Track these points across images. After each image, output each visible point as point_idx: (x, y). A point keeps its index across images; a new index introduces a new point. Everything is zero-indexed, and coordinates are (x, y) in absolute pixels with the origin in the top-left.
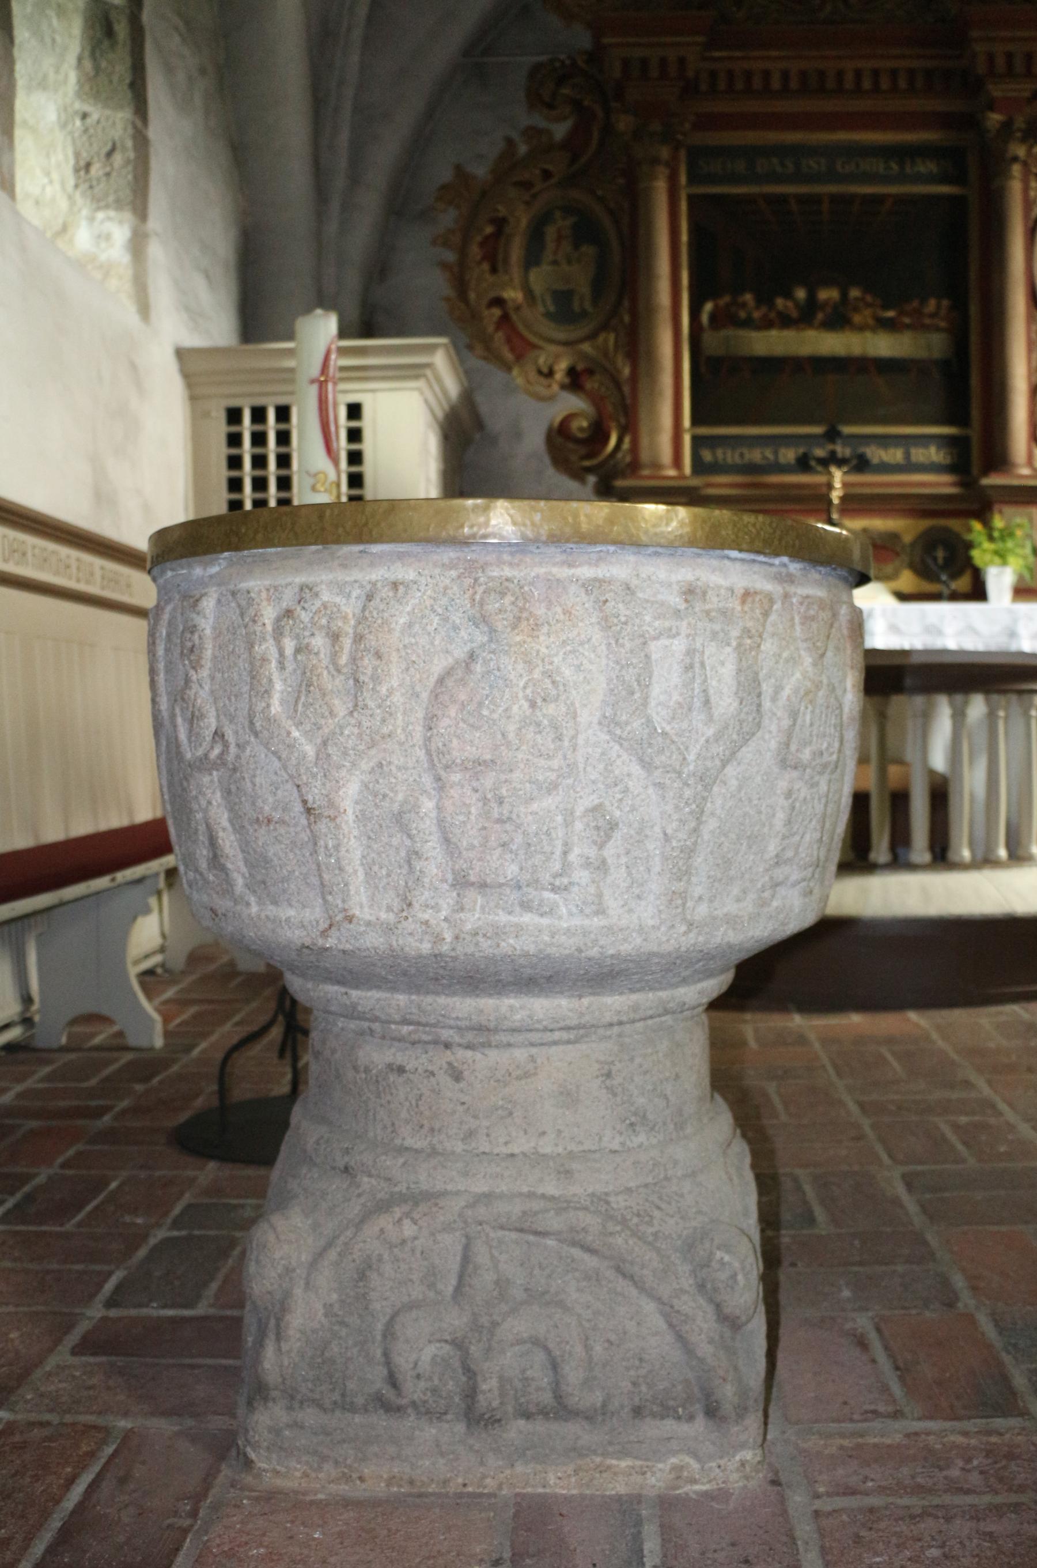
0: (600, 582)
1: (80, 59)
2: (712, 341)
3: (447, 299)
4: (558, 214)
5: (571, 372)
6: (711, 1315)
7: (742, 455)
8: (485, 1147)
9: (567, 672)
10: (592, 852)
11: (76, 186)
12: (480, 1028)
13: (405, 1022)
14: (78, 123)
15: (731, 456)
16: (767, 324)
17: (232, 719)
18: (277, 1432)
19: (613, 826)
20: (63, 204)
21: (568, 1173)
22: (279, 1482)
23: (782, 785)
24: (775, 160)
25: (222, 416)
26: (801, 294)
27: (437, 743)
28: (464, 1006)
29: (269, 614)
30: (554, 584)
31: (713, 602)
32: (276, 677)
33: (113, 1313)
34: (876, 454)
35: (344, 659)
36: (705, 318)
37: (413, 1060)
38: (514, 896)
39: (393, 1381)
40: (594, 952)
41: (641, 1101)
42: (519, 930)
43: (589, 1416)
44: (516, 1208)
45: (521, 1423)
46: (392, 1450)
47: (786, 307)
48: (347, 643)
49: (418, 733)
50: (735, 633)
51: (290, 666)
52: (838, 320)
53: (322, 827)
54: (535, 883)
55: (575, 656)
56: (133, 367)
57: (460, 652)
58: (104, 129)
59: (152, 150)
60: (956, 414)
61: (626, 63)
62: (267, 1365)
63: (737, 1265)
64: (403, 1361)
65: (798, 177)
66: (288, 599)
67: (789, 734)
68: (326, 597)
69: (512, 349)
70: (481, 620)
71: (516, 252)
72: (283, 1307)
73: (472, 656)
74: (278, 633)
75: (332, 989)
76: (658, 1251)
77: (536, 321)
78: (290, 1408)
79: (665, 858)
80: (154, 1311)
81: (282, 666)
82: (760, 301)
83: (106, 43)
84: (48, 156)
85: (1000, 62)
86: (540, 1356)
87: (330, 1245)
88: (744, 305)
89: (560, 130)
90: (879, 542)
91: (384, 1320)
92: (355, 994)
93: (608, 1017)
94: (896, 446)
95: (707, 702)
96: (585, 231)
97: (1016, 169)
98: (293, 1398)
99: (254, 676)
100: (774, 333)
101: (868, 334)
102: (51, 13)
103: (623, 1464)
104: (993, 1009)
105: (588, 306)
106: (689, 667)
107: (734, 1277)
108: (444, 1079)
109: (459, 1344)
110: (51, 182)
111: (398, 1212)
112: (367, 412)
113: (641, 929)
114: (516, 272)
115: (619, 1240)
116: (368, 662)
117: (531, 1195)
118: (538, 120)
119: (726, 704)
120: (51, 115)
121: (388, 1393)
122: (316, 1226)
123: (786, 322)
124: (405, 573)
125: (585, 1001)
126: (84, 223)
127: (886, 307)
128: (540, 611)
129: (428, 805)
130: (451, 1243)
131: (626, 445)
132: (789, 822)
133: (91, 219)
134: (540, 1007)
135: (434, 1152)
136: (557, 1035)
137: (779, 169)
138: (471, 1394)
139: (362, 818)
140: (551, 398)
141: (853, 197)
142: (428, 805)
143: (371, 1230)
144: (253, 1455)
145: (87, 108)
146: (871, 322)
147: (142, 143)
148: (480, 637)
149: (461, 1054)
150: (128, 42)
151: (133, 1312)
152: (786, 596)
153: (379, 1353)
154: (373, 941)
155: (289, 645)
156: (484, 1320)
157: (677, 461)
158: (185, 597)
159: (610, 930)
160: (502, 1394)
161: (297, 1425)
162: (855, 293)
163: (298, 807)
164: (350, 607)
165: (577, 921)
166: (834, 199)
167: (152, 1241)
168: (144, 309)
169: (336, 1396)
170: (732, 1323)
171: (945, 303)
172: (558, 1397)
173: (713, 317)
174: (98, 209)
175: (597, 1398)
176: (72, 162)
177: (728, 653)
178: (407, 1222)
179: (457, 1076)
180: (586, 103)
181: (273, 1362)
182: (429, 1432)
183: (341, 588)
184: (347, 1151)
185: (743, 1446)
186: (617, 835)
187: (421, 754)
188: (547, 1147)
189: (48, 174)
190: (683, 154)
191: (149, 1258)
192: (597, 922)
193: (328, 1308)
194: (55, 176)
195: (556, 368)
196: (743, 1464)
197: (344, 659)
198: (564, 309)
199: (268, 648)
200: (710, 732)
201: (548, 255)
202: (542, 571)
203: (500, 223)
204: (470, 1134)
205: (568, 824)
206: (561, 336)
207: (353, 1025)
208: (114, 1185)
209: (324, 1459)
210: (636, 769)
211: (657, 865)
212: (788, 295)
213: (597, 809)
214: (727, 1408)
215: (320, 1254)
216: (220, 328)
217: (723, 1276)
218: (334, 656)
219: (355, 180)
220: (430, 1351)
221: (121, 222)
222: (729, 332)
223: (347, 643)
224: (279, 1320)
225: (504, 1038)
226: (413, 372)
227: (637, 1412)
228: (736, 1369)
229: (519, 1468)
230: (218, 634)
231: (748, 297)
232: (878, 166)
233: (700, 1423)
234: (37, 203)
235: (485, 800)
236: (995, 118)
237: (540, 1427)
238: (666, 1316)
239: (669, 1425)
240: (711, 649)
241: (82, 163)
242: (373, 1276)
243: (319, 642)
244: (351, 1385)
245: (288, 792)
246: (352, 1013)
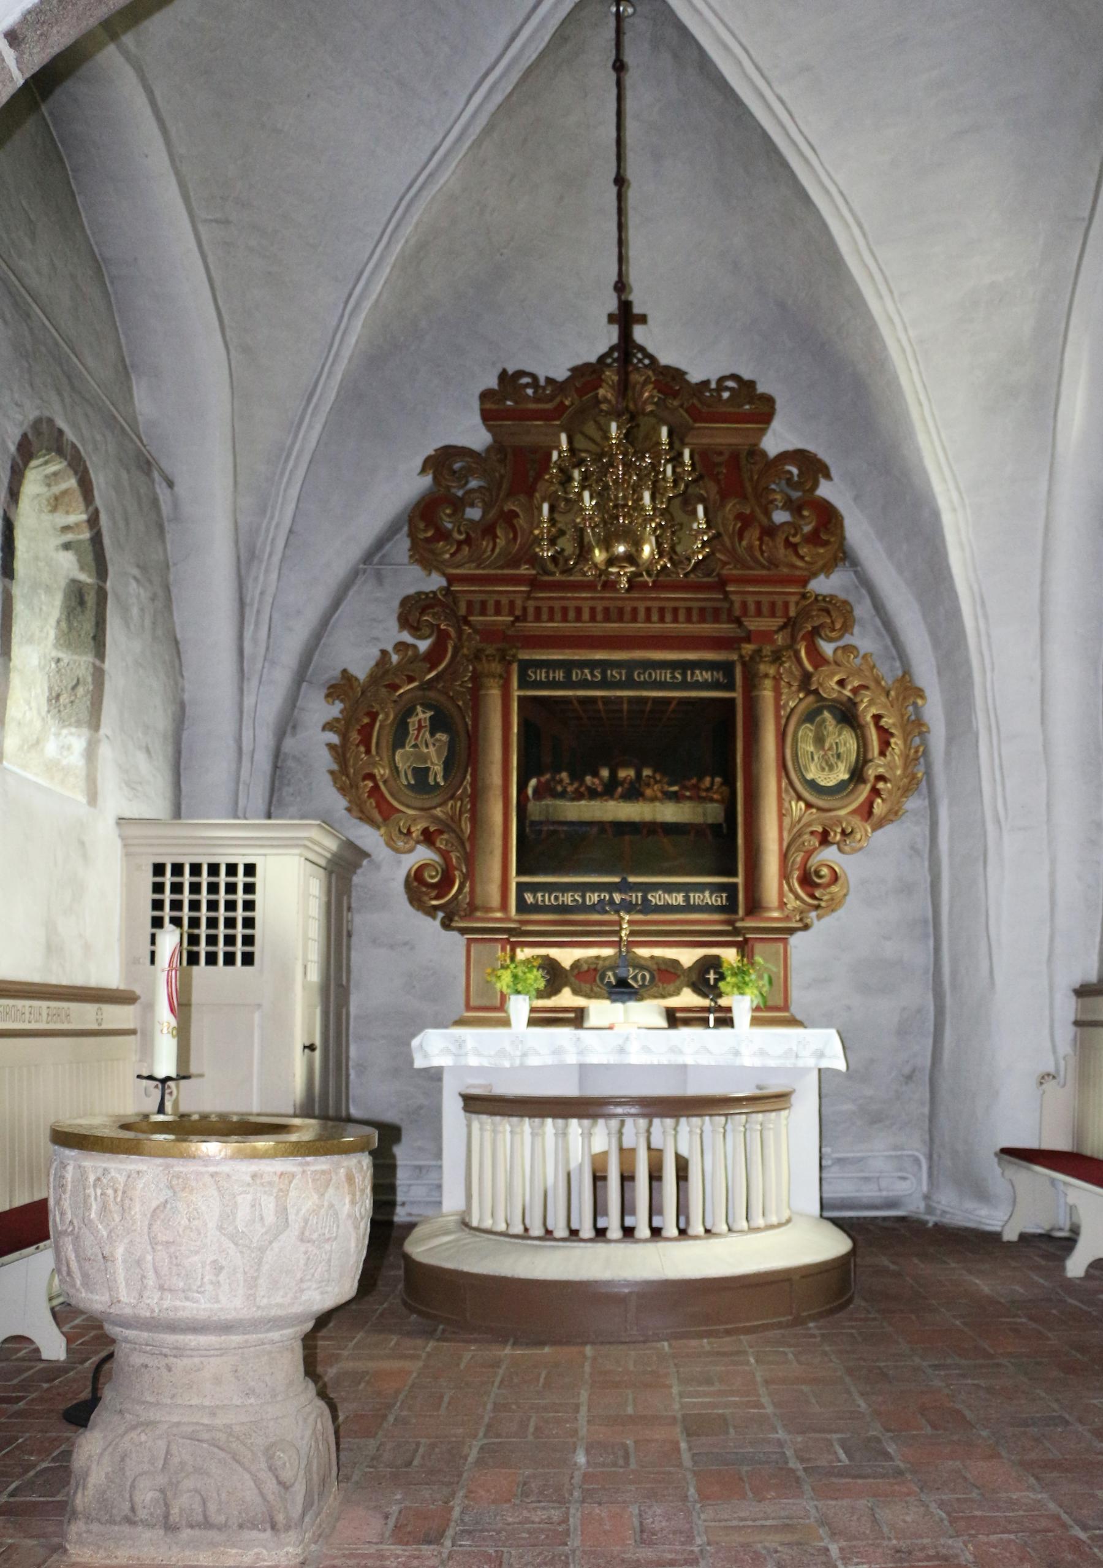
0: (216, 1173)
1: (58, 622)
2: (535, 809)
3: (332, 773)
4: (419, 709)
5: (425, 832)
6: (274, 1481)
7: (556, 898)
8: (179, 1402)
9: (203, 1208)
10: (214, 1279)
11: (49, 711)
12: (176, 1348)
13: (147, 1345)
14: (53, 665)
15: (548, 899)
16: (578, 796)
17: (77, 1216)
18: (79, 1534)
19: (222, 1268)
20: (38, 724)
21: (214, 1414)
22: (79, 1560)
23: (303, 1249)
24: (587, 671)
25: (150, 870)
26: (605, 773)
27: (152, 1235)
28: (170, 1338)
29: (92, 1178)
30: (199, 1174)
31: (266, 1179)
32: (94, 1204)
33: (12, 1499)
35: (119, 1199)
36: (530, 791)
37: (151, 1362)
38: (182, 1295)
39: (133, 1509)
40: (215, 1318)
41: (252, 1384)
42: (184, 1308)
43: (220, 1528)
44: (190, 1429)
45: (189, 1530)
46: (130, 1542)
47: (594, 784)
48: (120, 1193)
49: (146, 1230)
50: (275, 1190)
51: (99, 1199)
52: (633, 793)
53: (109, 1264)
54: (190, 1289)
55: (206, 1204)
56: (82, 843)
57: (162, 1200)
58: (71, 670)
59: (106, 677)
61: (470, 604)
62: (77, 1502)
63: (286, 1459)
64: (138, 1499)
65: (604, 684)
66: (100, 1172)
67: (304, 1228)
68: (113, 1174)
69: (380, 812)
70: (171, 1187)
72: (86, 1474)
73: (166, 1201)
74: (95, 1186)
75: (118, 1329)
76: (252, 1451)
78: (86, 1523)
79: (245, 1281)
80: (34, 1498)
81: (96, 1199)
82: (573, 777)
83: (79, 609)
84: (30, 690)
85: (752, 608)
86: (198, 1498)
87: (110, 1444)
88: (561, 781)
89: (423, 645)
90: (663, 967)
91: (131, 1480)
92: (127, 1332)
93: (233, 1345)
94: (678, 891)
95: (262, 1219)
97: (768, 683)
98: (89, 1519)
99: (85, 1202)
100: (583, 802)
101: (657, 804)
102: (41, 592)
103: (234, 1551)
105: (440, 780)
106: (253, 1206)
107: (285, 1464)
108: (164, 1371)
109: (162, 1491)
110: (31, 709)
111: (139, 1430)
112: (259, 870)
113: (235, 1309)
114: (385, 754)
115: (234, 1445)
116: (127, 1202)
117: (197, 1423)
118: (406, 637)
119: (270, 1218)
120: (34, 661)
121: (130, 1514)
122: (105, 1437)
123: (593, 794)
124: (142, 1167)
125: (223, 1338)
126: (52, 738)
127: (671, 784)
128: (194, 1184)
129: (149, 1258)
130: (162, 1444)
131: (467, 889)
132: (306, 1264)
133: (57, 735)
134: (203, 1340)
135: (158, 1404)
136: (212, 1352)
137: (589, 677)
138: (167, 1516)
139: (124, 1261)
140: (411, 851)
141: (647, 698)
142: (149, 1258)
143: (127, 1438)
144: (68, 1547)
145: (61, 655)
146: (659, 795)
147: (99, 675)
148: (170, 1193)
149: (172, 1360)
150: (95, 606)
151: (22, 1499)
152: (304, 1172)
153: (128, 1496)
154: (128, 1311)
155: (99, 1192)
156: (174, 1480)
157: (504, 906)
158: (62, 1163)
159: (222, 1309)
160: (181, 1516)
161: (89, 1531)
162: (647, 772)
163: (100, 1256)
164: (121, 1179)
165: (208, 1305)
166: (631, 700)
167: (38, 1469)
168: (93, 797)
169: (107, 1517)
170: (284, 1486)
171: (718, 780)
172: (205, 1517)
173: (536, 791)
174: (64, 727)
175: (222, 1519)
176: (47, 694)
177: (272, 1199)
178: (143, 1435)
179: (169, 1369)
180: (442, 627)
181: (82, 1500)
182: (147, 1534)
183: (119, 1171)
184: (121, 1403)
185: (288, 1544)
186: (224, 1272)
187: (146, 1237)
188: (207, 1403)
189: (29, 703)
190: (515, 667)
191: (36, 1475)
192: (216, 1306)
193: (107, 1474)
194: (33, 704)
195: (413, 829)
196: (287, 1553)
197: (119, 1199)
199: (91, 1191)
200: (263, 1230)
201: (410, 741)
202: (195, 1168)
204: (173, 1396)
205: (203, 1267)
206: (418, 804)
207: (128, 1346)
208: (20, 1440)
209: (99, 1547)
210: (232, 1246)
211: (242, 1283)
212: (595, 774)
213: (215, 1261)
214: (280, 1526)
215: (105, 1450)
216: (153, 804)
217: (279, 1463)
218: (115, 1198)
220: (150, 1495)
221: (79, 736)
222: (548, 801)
223: (120, 1193)
224: (84, 1480)
225: (189, 1353)
227: (241, 1526)
228: (286, 1508)
229: (187, 1553)
230: (73, 1182)
231: (564, 775)
232: (667, 675)
233: (269, 1532)
234: (19, 724)
235: (171, 1257)
237: (197, 1532)
238: (255, 1482)
239: (254, 1534)
240: (264, 1197)
241: (54, 694)
242: (128, 1460)
243: (110, 1192)
244: (115, 1511)
245: (97, 1250)
246: (126, 1340)
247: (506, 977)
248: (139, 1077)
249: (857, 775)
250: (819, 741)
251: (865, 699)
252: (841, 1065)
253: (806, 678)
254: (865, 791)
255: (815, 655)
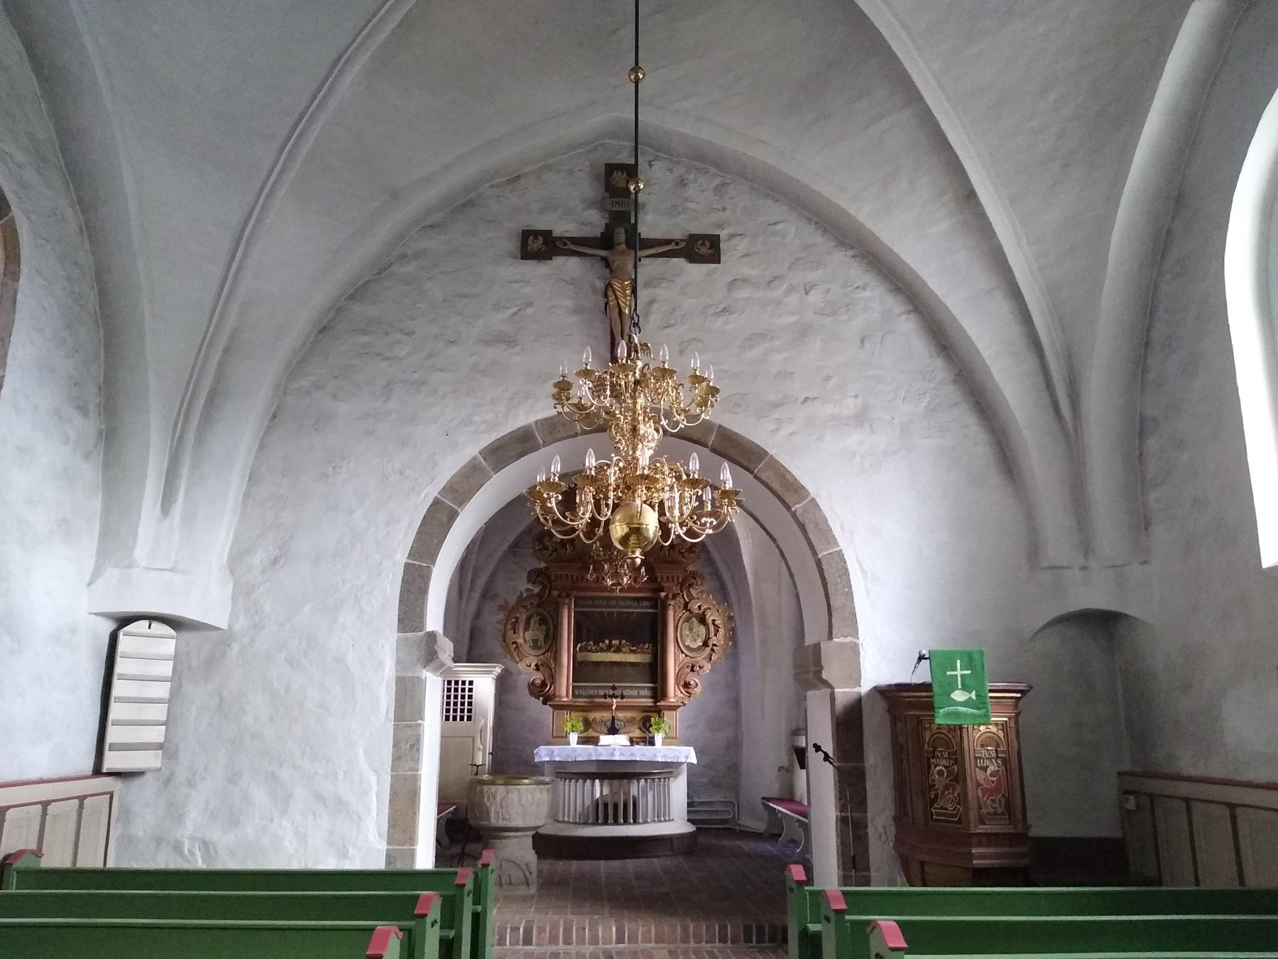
34: (625, 693)
52: (618, 650)
60: (653, 680)
71: (522, 627)
77: (526, 649)
89: (537, 590)
96: (543, 621)
104: (91, 571)
118: (530, 586)
123: (602, 650)
198: (535, 645)
203: (517, 619)
219: (471, 590)
226: (489, 673)
232: (629, 603)
236: (663, 594)
247: (569, 725)
248: (89, 584)
249: (705, 644)
250: (691, 629)
251: (708, 614)
252: (695, 761)
253: (686, 604)
254: (708, 649)
255: (689, 594)
